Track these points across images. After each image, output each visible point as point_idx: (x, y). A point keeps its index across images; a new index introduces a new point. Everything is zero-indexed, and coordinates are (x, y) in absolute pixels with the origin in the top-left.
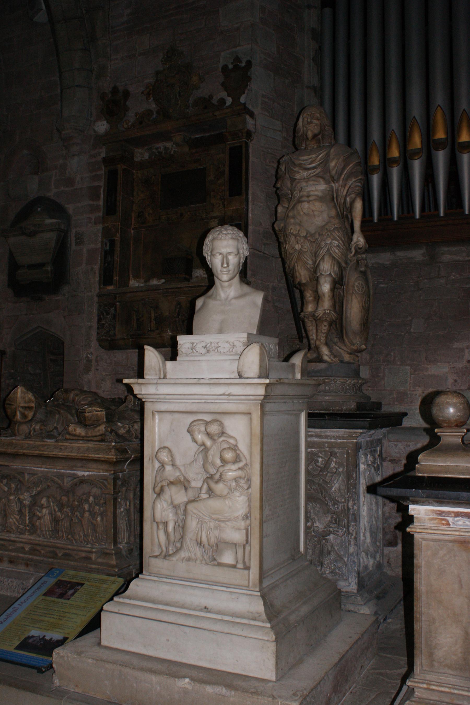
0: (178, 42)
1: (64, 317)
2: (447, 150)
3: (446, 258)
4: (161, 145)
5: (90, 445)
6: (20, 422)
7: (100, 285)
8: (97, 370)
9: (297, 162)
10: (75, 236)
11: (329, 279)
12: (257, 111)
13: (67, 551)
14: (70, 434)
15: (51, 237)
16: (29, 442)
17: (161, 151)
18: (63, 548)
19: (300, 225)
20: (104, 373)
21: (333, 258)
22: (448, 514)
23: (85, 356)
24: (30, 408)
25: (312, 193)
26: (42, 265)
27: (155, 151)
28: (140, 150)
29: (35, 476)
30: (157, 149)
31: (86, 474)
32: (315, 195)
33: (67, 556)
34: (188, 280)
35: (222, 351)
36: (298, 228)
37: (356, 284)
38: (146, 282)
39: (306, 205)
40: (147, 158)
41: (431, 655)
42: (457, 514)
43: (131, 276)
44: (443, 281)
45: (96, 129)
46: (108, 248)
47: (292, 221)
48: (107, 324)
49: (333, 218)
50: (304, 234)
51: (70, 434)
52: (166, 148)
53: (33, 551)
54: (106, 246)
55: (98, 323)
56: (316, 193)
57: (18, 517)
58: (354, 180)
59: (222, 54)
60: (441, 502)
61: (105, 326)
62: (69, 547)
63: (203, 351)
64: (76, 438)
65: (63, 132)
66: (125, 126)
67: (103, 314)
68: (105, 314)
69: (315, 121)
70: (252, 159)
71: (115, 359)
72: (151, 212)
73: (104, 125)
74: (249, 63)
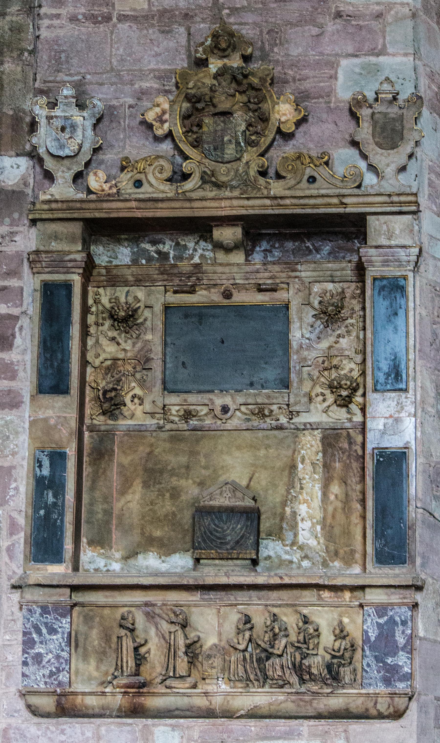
0: (227, 11)
17: (165, 250)
38: (126, 558)
48: (50, 656)
54: (40, 466)
55: (24, 652)
59: (344, 62)
61: (47, 660)
67: (39, 632)
68: (44, 631)
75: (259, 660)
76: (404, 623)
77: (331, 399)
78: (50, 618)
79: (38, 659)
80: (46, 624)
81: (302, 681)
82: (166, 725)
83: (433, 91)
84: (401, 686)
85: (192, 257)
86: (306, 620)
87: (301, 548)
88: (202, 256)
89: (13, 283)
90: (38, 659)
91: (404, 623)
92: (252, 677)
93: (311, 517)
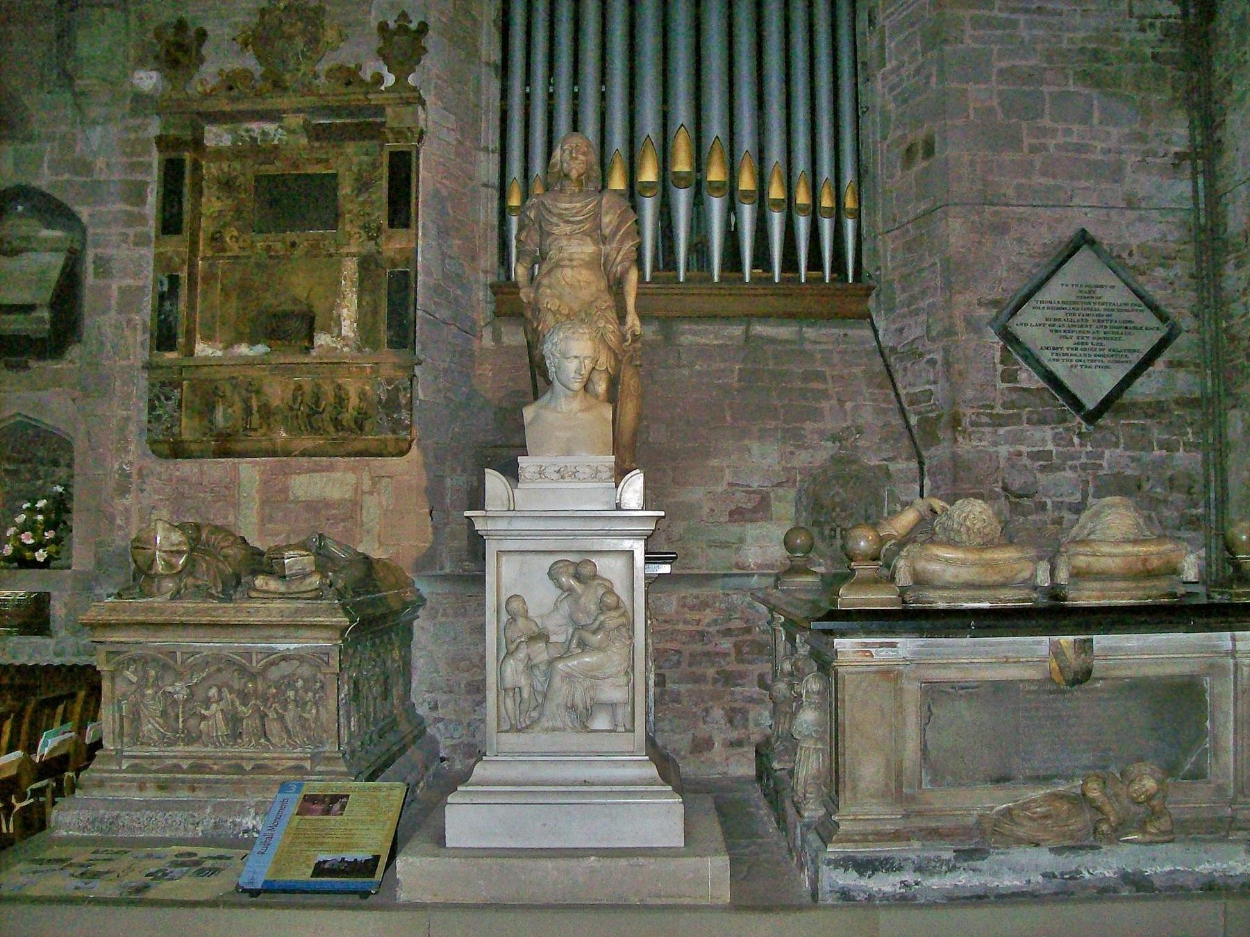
1: (74, 400)
2: (692, 189)
3: (686, 339)
4: (256, 127)
5: (299, 605)
6: (162, 575)
7: (151, 349)
8: (142, 491)
9: (556, 211)
10: (94, 262)
11: (604, 376)
12: (429, 99)
13: (259, 762)
14: (257, 590)
15: (55, 262)
16: (185, 605)
18: (251, 759)
19: (560, 298)
20: (156, 497)
21: (610, 348)
22: (873, 645)
23: (116, 466)
24: (180, 553)
25: (576, 256)
26: (27, 309)
27: (243, 133)
28: (214, 129)
29: (198, 656)
30: (247, 131)
31: (292, 647)
32: (581, 259)
33: (258, 768)
34: (307, 350)
35: (581, 477)
36: (557, 302)
37: (632, 382)
38: (226, 348)
39: (568, 272)
40: (229, 144)
41: (854, 788)
42: (881, 645)
43: (198, 336)
44: (686, 372)
45: (136, 81)
46: (166, 288)
47: (548, 291)
49: (602, 291)
50: (567, 312)
51: (257, 590)
52: (264, 133)
53: (198, 768)
55: (149, 413)
56: (582, 256)
57: (161, 721)
58: (631, 243)
60: (869, 633)
62: (265, 755)
63: (555, 476)
64: (271, 596)
65: (78, 82)
66: (200, 89)
68: (163, 398)
69: (581, 157)
70: (422, 173)
71: (178, 473)
72: (235, 233)
73: (151, 78)
74: (423, 28)
75: (308, 416)
76: (405, 389)
77: (364, 236)
78: (167, 390)
79: (159, 417)
80: (163, 393)
81: (337, 431)
82: (247, 463)
83: (442, 22)
84: (403, 434)
85: (273, 140)
86: (339, 387)
87: (343, 339)
88: (279, 139)
89: (145, 159)
90: (159, 417)
91: (405, 389)
92: (303, 428)
93: (350, 317)
